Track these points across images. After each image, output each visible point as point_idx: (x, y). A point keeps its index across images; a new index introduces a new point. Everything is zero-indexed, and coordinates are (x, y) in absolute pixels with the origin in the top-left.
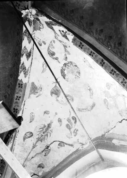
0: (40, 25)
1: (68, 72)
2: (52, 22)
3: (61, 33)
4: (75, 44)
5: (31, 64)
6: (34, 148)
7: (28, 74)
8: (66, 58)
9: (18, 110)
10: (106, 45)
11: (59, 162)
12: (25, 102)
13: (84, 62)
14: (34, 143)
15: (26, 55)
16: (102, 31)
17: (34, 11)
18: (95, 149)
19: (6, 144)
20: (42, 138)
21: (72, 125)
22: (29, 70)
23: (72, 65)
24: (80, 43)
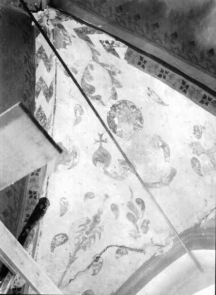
0: (66, 40)
1: (121, 121)
2: (87, 28)
3: (104, 46)
4: (130, 61)
7: (50, 128)
8: (115, 94)
9: (38, 193)
10: (187, 58)
12: (48, 178)
13: (148, 96)
14: (72, 253)
15: (44, 93)
17: (53, 13)
20: (84, 242)
21: (137, 215)
24: (139, 58)
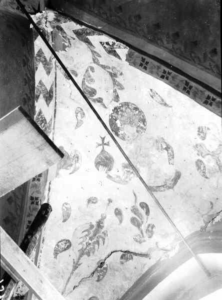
0: (64, 41)
2: (86, 29)
3: (105, 47)
5: (55, 113)
6: (76, 269)
7: (50, 132)
9: (39, 199)
10: (191, 59)
11: (126, 290)
12: (50, 183)
16: (177, 35)
17: (51, 15)
18: (193, 254)
19: (25, 252)
21: (141, 219)
22: (53, 123)
23: (129, 108)
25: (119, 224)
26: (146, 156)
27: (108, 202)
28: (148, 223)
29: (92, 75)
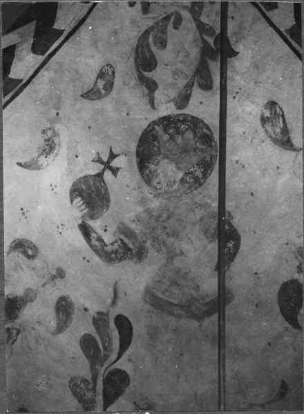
21: (105, 349)
25: (53, 334)
26: (173, 235)
27: (54, 272)
28: (118, 365)
29: (169, 33)
